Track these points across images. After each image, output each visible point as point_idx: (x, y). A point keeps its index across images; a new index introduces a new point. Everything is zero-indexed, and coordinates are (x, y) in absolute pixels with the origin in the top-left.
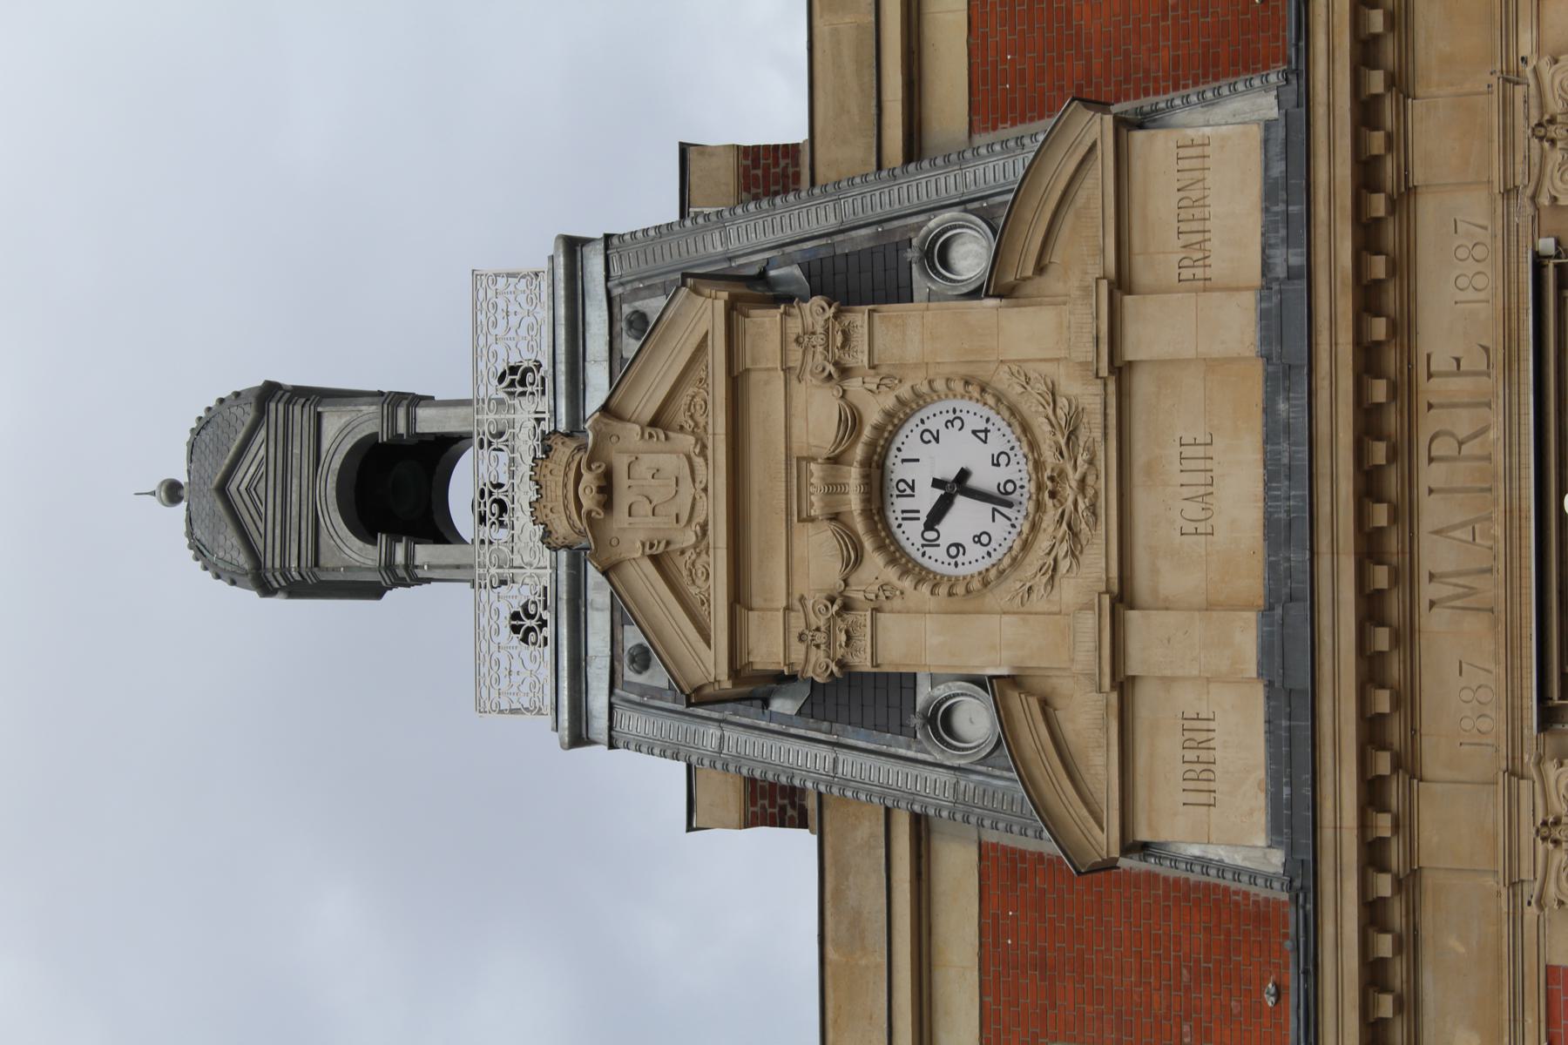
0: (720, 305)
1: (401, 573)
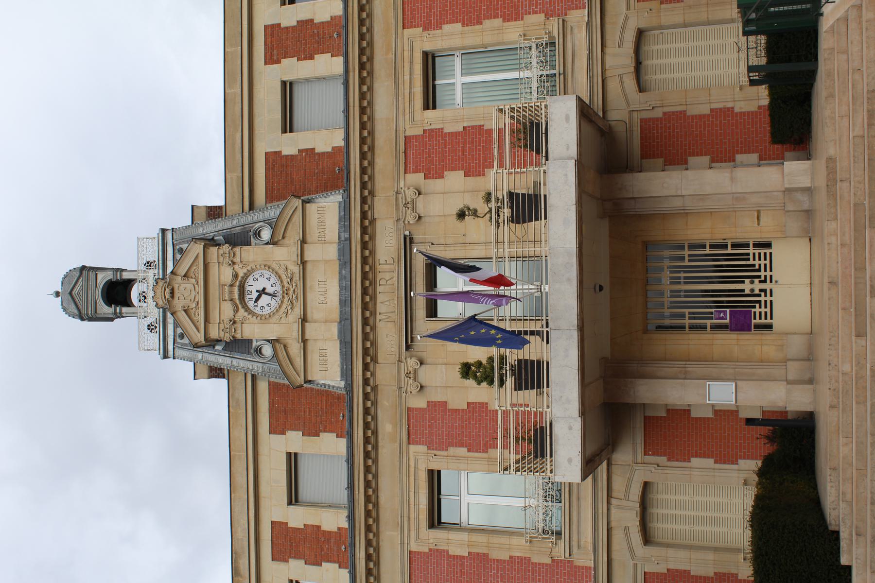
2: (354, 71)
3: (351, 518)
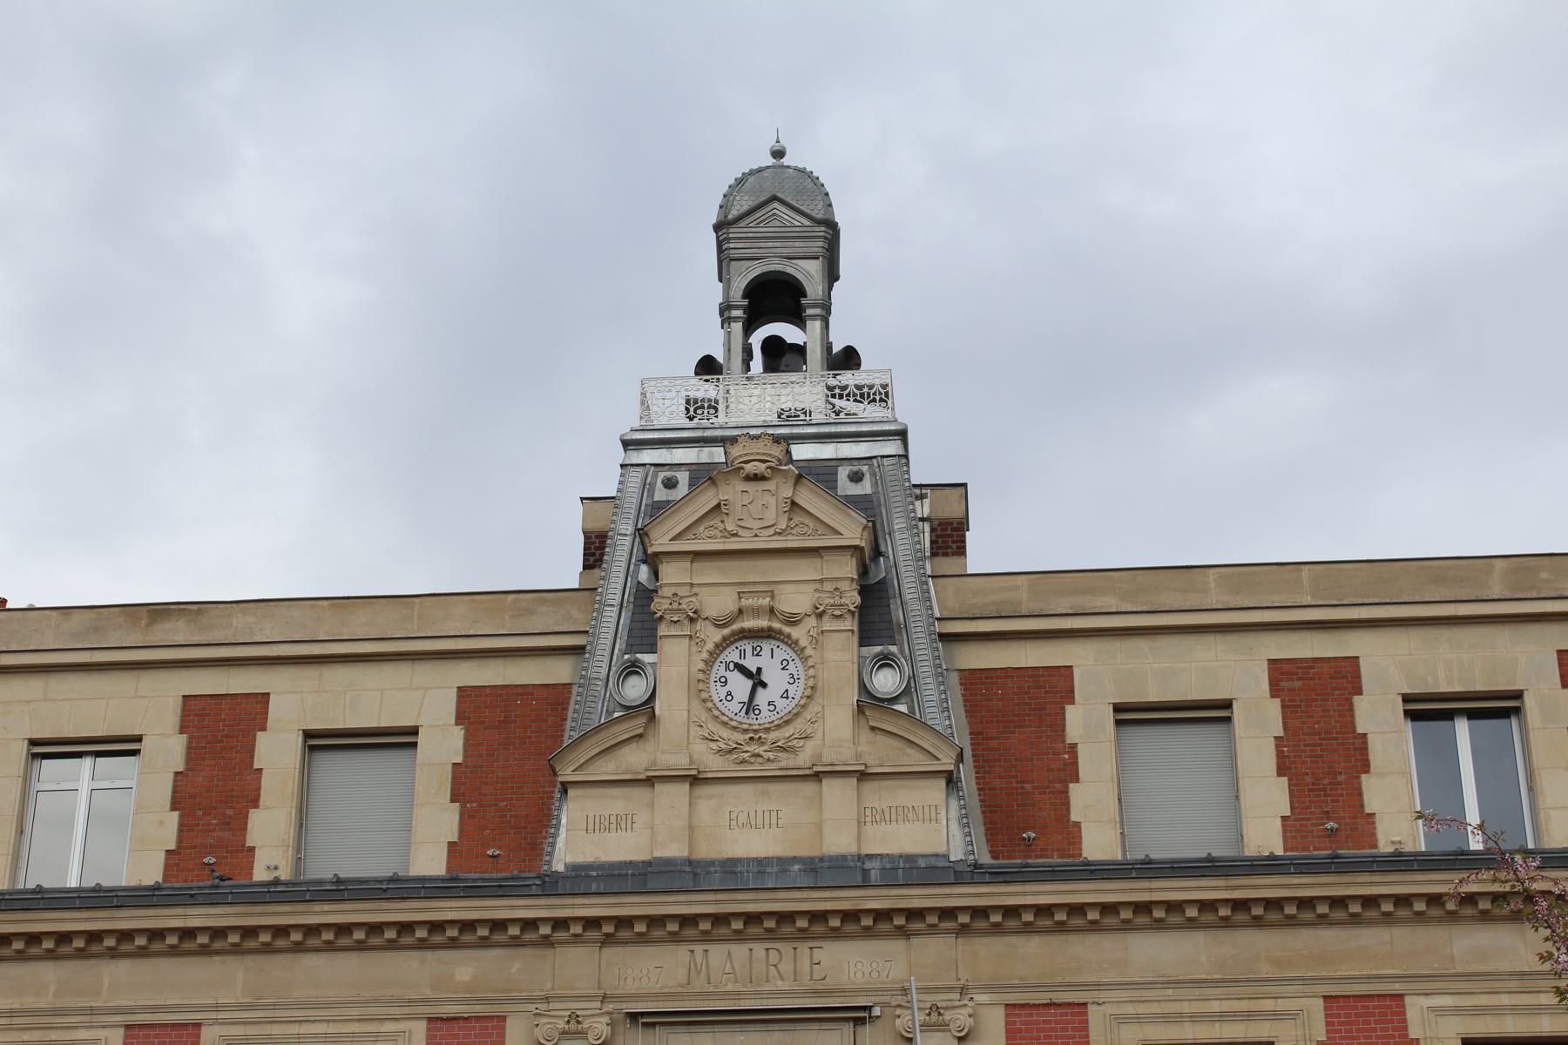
0: (857, 542)
1: (726, 314)
2: (1227, 888)
3: (275, 892)
